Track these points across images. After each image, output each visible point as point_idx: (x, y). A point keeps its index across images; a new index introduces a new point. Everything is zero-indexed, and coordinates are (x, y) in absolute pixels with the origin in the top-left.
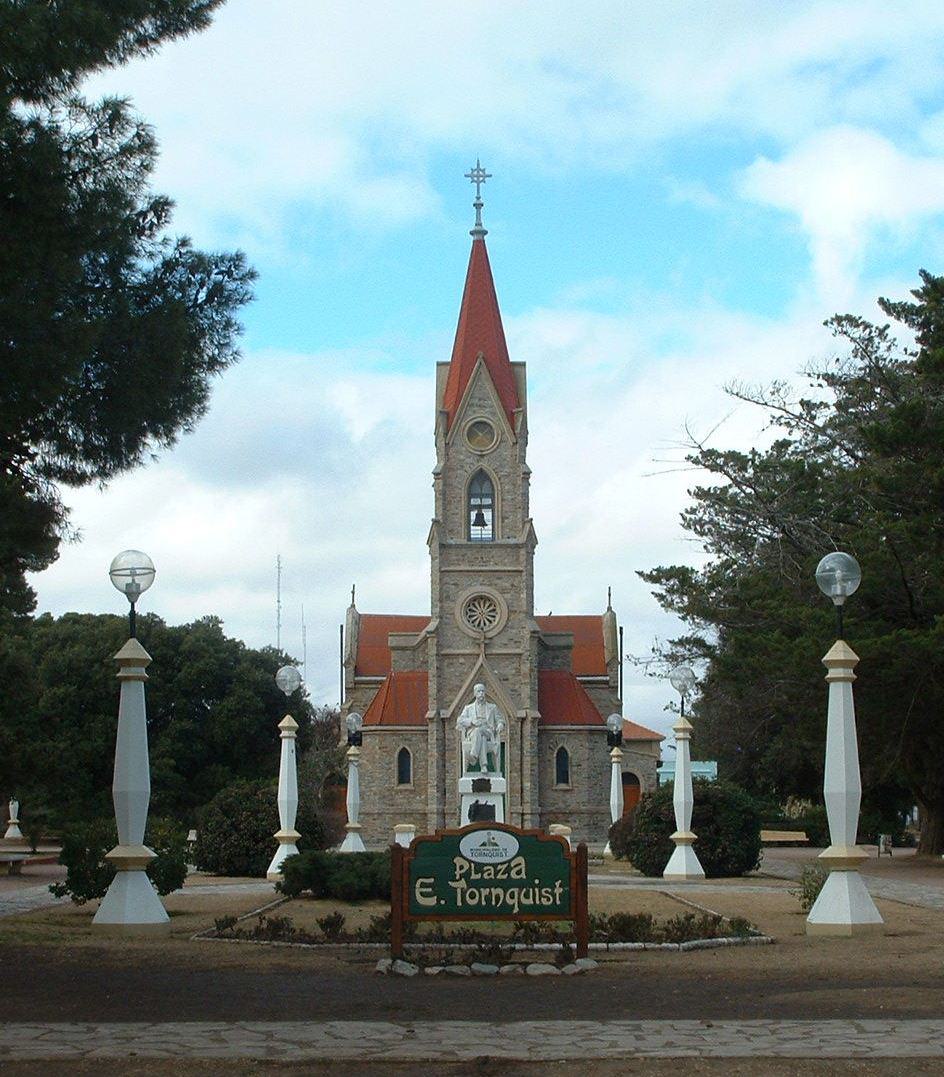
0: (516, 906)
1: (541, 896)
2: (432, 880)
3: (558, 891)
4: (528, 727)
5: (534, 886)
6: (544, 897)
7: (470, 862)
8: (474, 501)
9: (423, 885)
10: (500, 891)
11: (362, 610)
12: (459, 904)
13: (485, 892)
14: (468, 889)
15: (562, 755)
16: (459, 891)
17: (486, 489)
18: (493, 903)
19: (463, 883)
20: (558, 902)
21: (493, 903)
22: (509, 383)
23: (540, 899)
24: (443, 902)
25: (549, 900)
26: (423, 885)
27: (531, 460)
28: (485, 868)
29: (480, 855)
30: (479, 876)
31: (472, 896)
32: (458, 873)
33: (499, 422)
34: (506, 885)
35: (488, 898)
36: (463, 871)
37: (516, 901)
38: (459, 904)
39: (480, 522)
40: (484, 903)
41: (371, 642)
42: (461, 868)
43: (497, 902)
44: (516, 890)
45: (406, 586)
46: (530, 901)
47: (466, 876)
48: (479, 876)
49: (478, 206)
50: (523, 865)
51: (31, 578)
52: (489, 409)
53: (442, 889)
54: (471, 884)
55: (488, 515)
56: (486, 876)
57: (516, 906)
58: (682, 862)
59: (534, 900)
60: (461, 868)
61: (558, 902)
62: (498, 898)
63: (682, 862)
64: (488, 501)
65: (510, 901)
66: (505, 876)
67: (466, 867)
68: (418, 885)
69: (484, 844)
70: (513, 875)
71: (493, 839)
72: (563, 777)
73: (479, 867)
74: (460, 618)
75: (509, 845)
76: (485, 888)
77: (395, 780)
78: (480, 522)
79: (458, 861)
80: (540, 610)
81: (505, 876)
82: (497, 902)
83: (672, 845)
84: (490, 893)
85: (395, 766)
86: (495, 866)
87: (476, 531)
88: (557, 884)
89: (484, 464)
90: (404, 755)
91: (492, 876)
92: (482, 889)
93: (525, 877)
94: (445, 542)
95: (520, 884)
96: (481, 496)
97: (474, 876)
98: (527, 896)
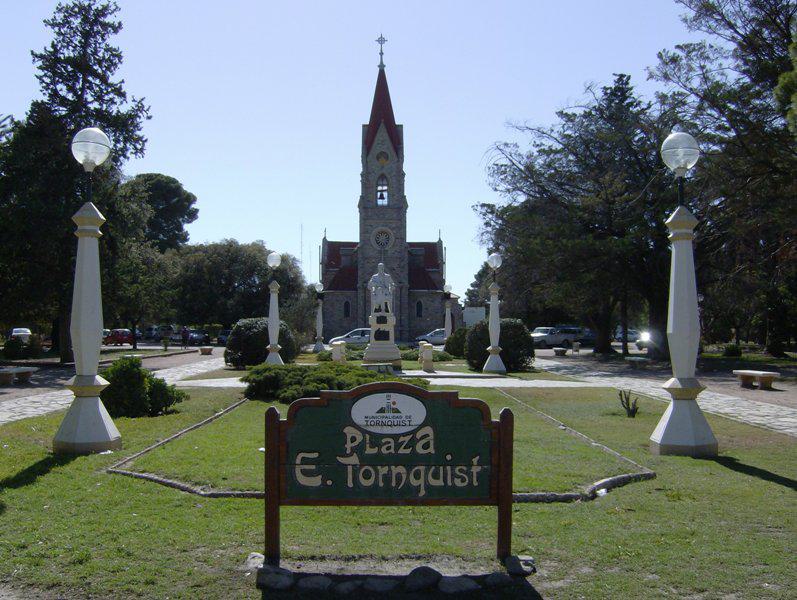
0: (422, 487)
1: (454, 476)
2: (316, 455)
3: (476, 469)
4: (403, 291)
5: (446, 463)
6: (459, 477)
7: (364, 432)
8: (380, 188)
9: (305, 461)
10: (401, 469)
11: (329, 239)
12: (350, 484)
13: (384, 470)
14: (362, 466)
15: (419, 305)
16: (350, 469)
17: (385, 182)
18: (394, 484)
19: (354, 460)
20: (475, 484)
21: (394, 484)
22: (395, 135)
23: (453, 480)
24: (329, 483)
25: (463, 480)
26: (305, 461)
27: (406, 168)
28: (383, 441)
29: (377, 424)
30: (375, 451)
31: (367, 475)
32: (349, 446)
33: (391, 152)
34: (409, 462)
35: (387, 478)
36: (356, 443)
37: (421, 482)
38: (350, 484)
39: (382, 197)
40: (381, 484)
41: (333, 253)
42: (353, 439)
43: (398, 484)
44: (422, 468)
45: (349, 231)
46: (440, 483)
47: (359, 450)
48: (375, 451)
49: (381, 54)
50: (432, 436)
51: (187, 227)
52: (387, 147)
53: (328, 466)
54: (365, 460)
55: (385, 194)
56: (384, 450)
57: (422, 487)
58: (493, 361)
59: (445, 480)
60: (353, 439)
61: (475, 484)
62: (399, 476)
63: (493, 361)
64: (385, 188)
65: (414, 482)
66: (408, 451)
67: (359, 438)
68: (298, 461)
69: (382, 411)
70: (419, 449)
71: (394, 403)
72: (419, 314)
73: (376, 440)
74: (373, 241)
75: (414, 411)
76: (382, 466)
77: (343, 315)
78: (382, 197)
79: (349, 431)
80: (409, 239)
81: (408, 451)
82: (398, 484)
83: (488, 354)
84: (390, 470)
85: (342, 309)
86: (395, 437)
87: (380, 202)
88: (475, 460)
89: (384, 171)
90: (347, 305)
91: (392, 451)
92: (379, 467)
93: (433, 452)
94: (367, 206)
95: (426, 460)
96: (383, 185)
97: (370, 451)
98: (436, 476)
